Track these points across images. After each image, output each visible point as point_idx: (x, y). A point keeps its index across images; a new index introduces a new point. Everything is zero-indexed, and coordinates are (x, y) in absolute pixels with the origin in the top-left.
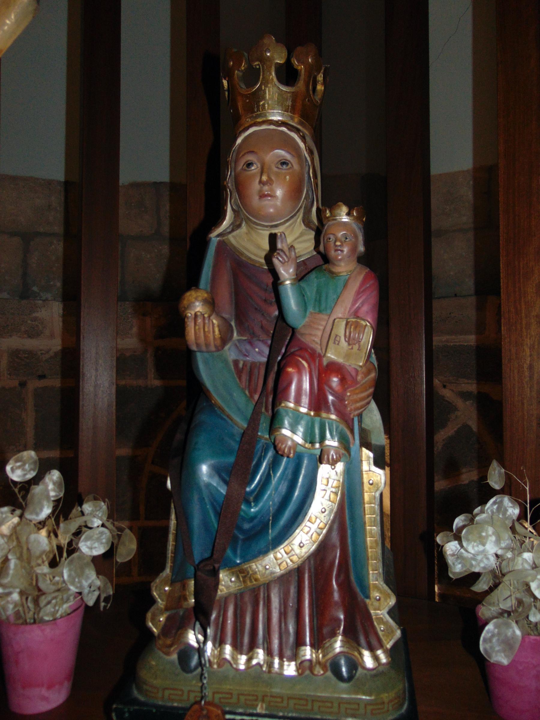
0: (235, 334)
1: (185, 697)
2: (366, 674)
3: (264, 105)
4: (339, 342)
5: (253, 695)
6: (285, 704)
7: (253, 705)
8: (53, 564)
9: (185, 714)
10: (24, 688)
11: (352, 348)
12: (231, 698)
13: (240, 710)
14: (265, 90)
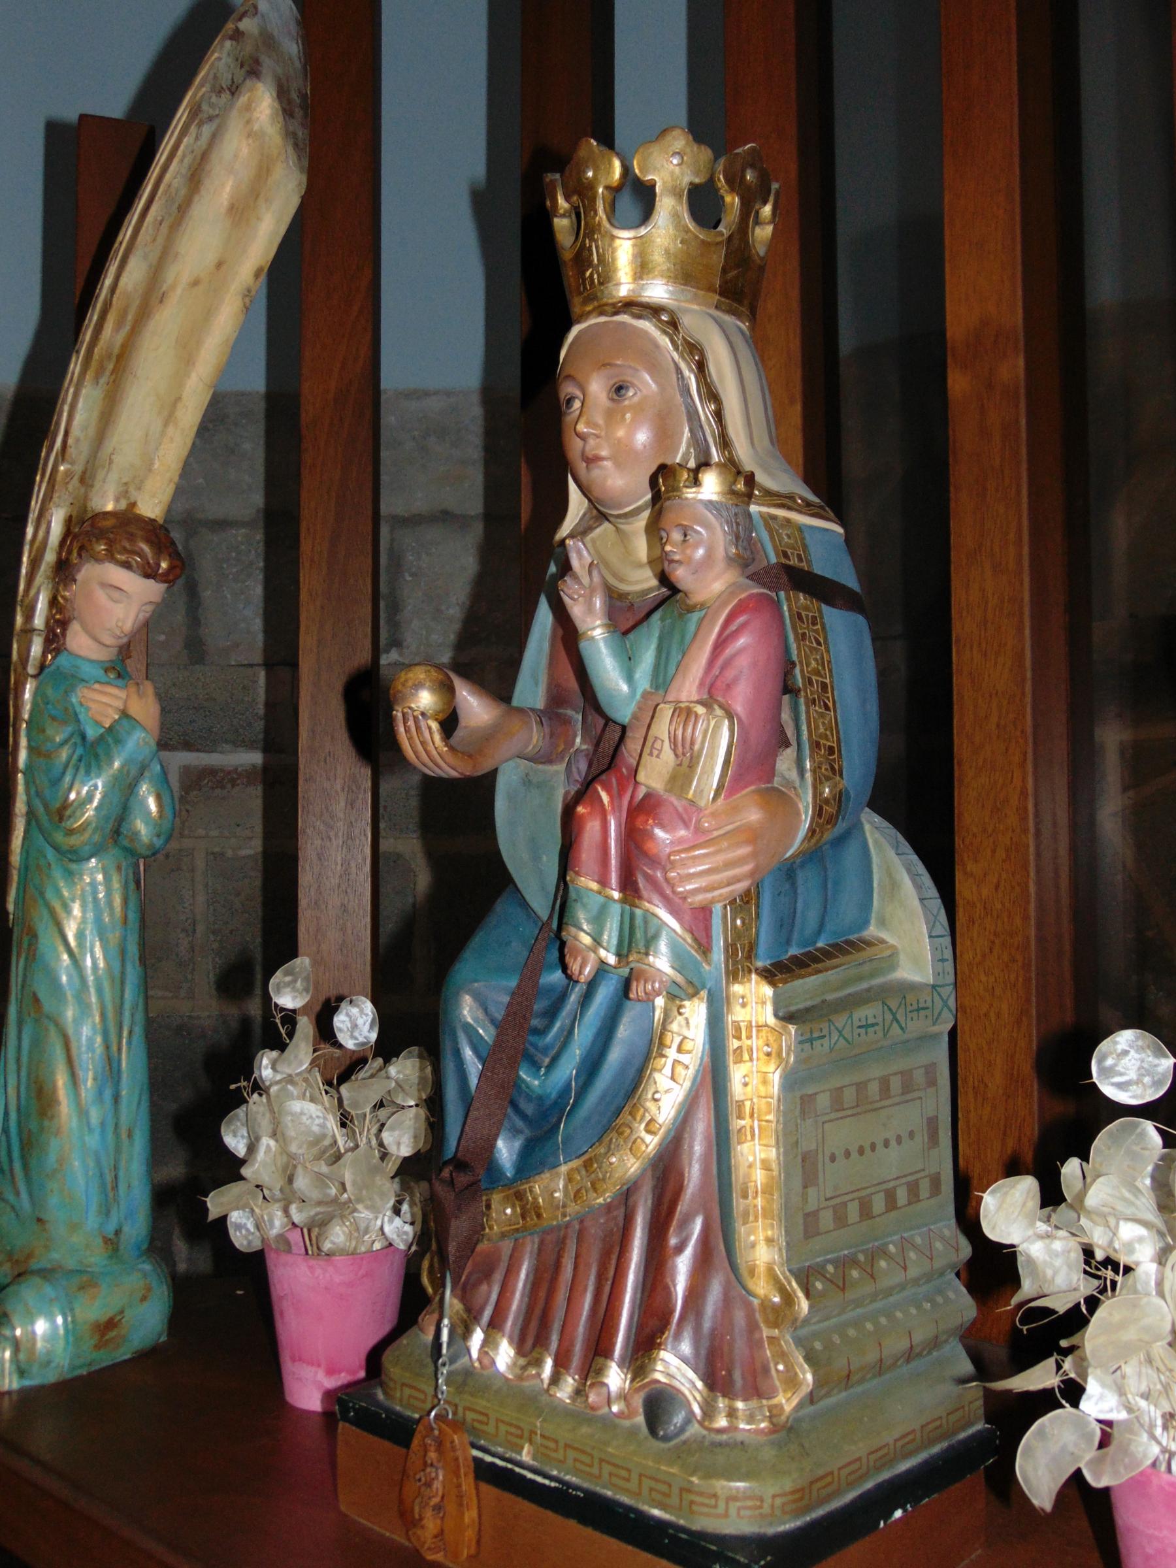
0: (578, 740)
2: (704, 1437)
3: (592, 275)
4: (660, 751)
6: (560, 1455)
7: (516, 1445)
10: (293, 1360)
13: (500, 1450)
14: (590, 246)
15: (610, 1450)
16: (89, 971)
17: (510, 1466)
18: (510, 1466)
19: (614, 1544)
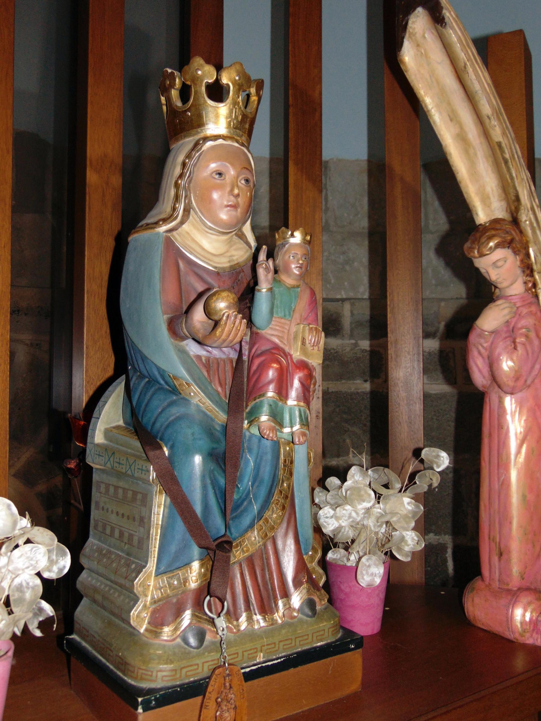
1: (200, 670)
5: (254, 649)
8: (387, 522)
9: (208, 683)
11: (313, 349)
12: (237, 657)
15: (299, 632)
16: (116, 446)
17: (259, 666)
18: (259, 666)
19: (338, 656)
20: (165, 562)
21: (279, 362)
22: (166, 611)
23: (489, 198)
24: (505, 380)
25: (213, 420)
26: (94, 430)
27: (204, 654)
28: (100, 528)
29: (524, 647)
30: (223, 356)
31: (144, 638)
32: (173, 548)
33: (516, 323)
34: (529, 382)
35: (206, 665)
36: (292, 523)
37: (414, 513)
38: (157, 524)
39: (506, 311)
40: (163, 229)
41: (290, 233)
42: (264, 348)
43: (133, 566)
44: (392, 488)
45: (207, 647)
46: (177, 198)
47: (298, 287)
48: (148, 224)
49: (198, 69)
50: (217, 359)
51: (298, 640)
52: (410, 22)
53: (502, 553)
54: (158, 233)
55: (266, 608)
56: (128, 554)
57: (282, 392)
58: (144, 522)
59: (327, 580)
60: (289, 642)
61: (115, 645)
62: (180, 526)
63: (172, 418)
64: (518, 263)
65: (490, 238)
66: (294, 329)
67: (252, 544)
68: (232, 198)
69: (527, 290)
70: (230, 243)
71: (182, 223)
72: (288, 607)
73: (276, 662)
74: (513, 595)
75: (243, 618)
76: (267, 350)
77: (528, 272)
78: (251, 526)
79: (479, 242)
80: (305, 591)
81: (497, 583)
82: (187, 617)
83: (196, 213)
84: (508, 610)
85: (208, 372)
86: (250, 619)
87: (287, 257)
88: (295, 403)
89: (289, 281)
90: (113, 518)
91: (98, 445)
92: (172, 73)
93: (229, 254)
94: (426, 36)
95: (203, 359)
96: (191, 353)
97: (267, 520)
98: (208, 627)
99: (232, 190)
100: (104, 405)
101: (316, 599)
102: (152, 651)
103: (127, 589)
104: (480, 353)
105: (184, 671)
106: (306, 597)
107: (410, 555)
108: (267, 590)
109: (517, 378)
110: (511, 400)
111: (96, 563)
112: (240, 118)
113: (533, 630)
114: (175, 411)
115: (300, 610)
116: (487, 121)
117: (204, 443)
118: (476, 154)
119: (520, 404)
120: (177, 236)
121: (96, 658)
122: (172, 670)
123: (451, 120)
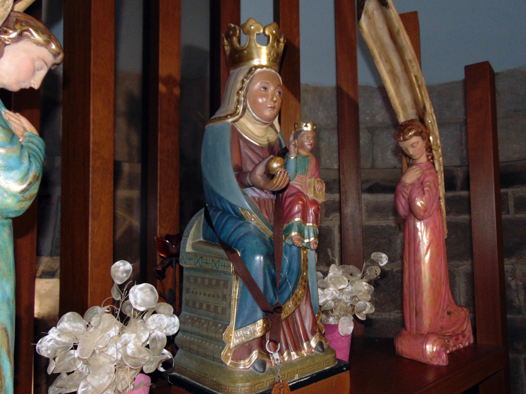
1: (265, 385)
20: (241, 321)
21: (303, 201)
22: (244, 350)
23: (406, 107)
24: (418, 211)
25: (264, 235)
26: (185, 244)
27: (266, 376)
28: (191, 304)
29: (433, 366)
30: (268, 197)
31: (230, 369)
32: (246, 313)
33: (423, 179)
34: (431, 213)
35: (268, 383)
36: (308, 297)
37: (369, 291)
38: (235, 299)
39: (418, 172)
40: (230, 120)
41: (305, 124)
42: (292, 192)
43: (220, 325)
44: (354, 276)
45: (267, 372)
46: (238, 101)
47: (309, 156)
48: (220, 117)
49: (252, 26)
50: (264, 199)
51: (316, 366)
52: (366, 4)
53: (418, 313)
54: (228, 123)
55: (298, 348)
56: (214, 318)
57: (304, 219)
58: (226, 298)
59: (325, 331)
60: (311, 367)
61: (209, 374)
62: (250, 298)
63: (242, 234)
64: (424, 145)
65: (410, 130)
66: (308, 181)
67: (290, 309)
68: (272, 103)
69: (428, 160)
70: (266, 130)
71: (241, 117)
72: (309, 346)
73: (305, 379)
74: (425, 337)
75: (285, 354)
76: (295, 193)
77: (429, 150)
78: (289, 298)
79: (403, 132)
80: (318, 337)
81: (415, 331)
82: (255, 355)
83: (249, 111)
84: (423, 346)
85: (260, 206)
86: (289, 354)
87: (303, 139)
88: (311, 224)
89: (303, 152)
90: (202, 298)
91: (189, 253)
92: (235, 28)
93: (266, 136)
94: (375, 12)
95: (256, 199)
96: (249, 195)
97: (296, 295)
98: (266, 359)
99: (272, 98)
100: (191, 229)
101: (324, 342)
102: (236, 376)
103: (216, 340)
104: (403, 196)
105: (256, 386)
106: (318, 340)
107: (365, 316)
108: (297, 337)
109: (425, 211)
110: (421, 224)
111: (190, 326)
112: (275, 55)
113: (438, 356)
114: (243, 231)
115: (316, 349)
116: (409, 63)
117: (263, 248)
118: (399, 82)
119: (426, 226)
120: (238, 125)
121: (195, 384)
122: (250, 386)
123: (387, 62)
